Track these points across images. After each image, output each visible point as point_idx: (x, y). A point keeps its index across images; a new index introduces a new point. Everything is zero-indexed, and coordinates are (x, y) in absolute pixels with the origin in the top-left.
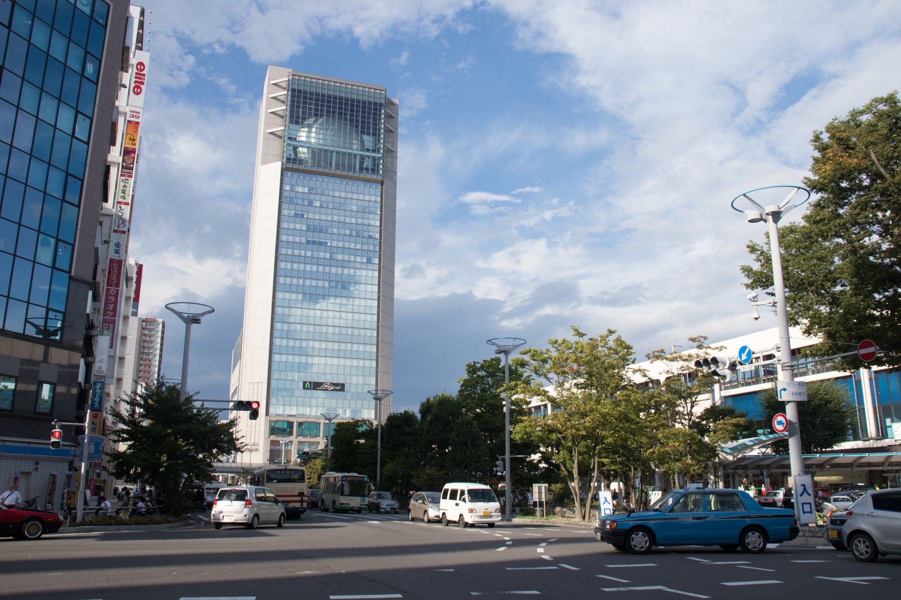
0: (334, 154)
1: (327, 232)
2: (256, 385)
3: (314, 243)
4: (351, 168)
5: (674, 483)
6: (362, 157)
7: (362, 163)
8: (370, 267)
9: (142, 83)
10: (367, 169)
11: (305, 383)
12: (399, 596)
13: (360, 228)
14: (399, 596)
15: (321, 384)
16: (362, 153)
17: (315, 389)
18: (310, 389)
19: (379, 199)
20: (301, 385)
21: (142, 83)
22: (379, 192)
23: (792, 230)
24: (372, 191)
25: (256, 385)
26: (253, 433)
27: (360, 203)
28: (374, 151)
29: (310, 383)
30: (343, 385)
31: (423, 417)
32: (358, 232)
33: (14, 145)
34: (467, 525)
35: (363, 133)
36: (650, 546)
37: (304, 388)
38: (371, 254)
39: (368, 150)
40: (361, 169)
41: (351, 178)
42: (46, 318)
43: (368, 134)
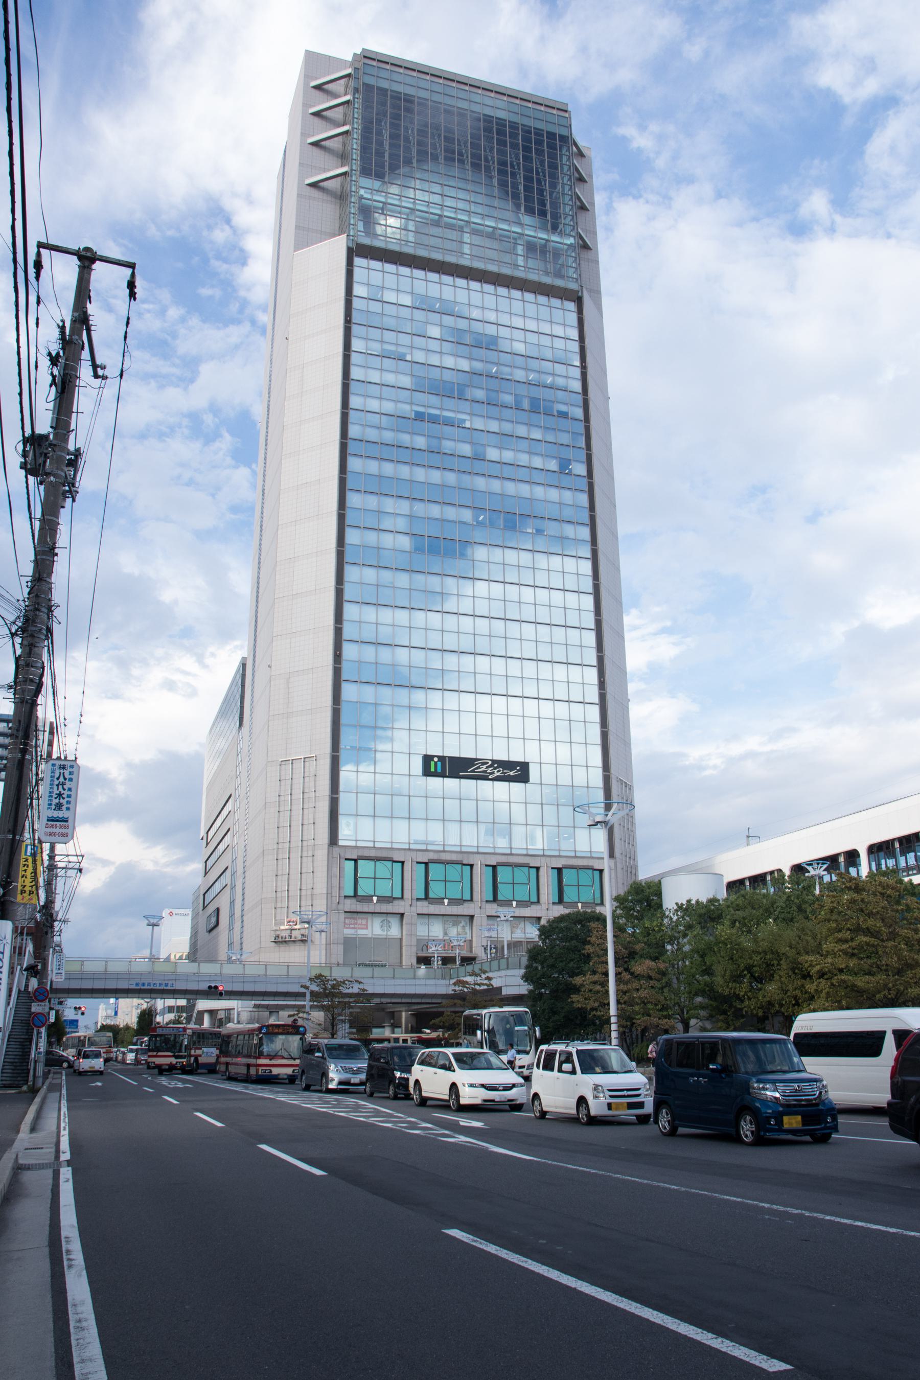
1: (461, 398)
2: (299, 766)
3: (434, 420)
8: (566, 481)
11: (427, 759)
13: (540, 393)
15: (469, 762)
17: (454, 775)
18: (442, 775)
19: (574, 334)
20: (417, 765)
22: (573, 318)
23: (544, 926)
24: (558, 315)
25: (299, 766)
26: (298, 795)
27: (532, 338)
29: (442, 759)
31: (544, 941)
32: (535, 402)
34: (594, 1121)
37: (427, 772)
38: (569, 454)
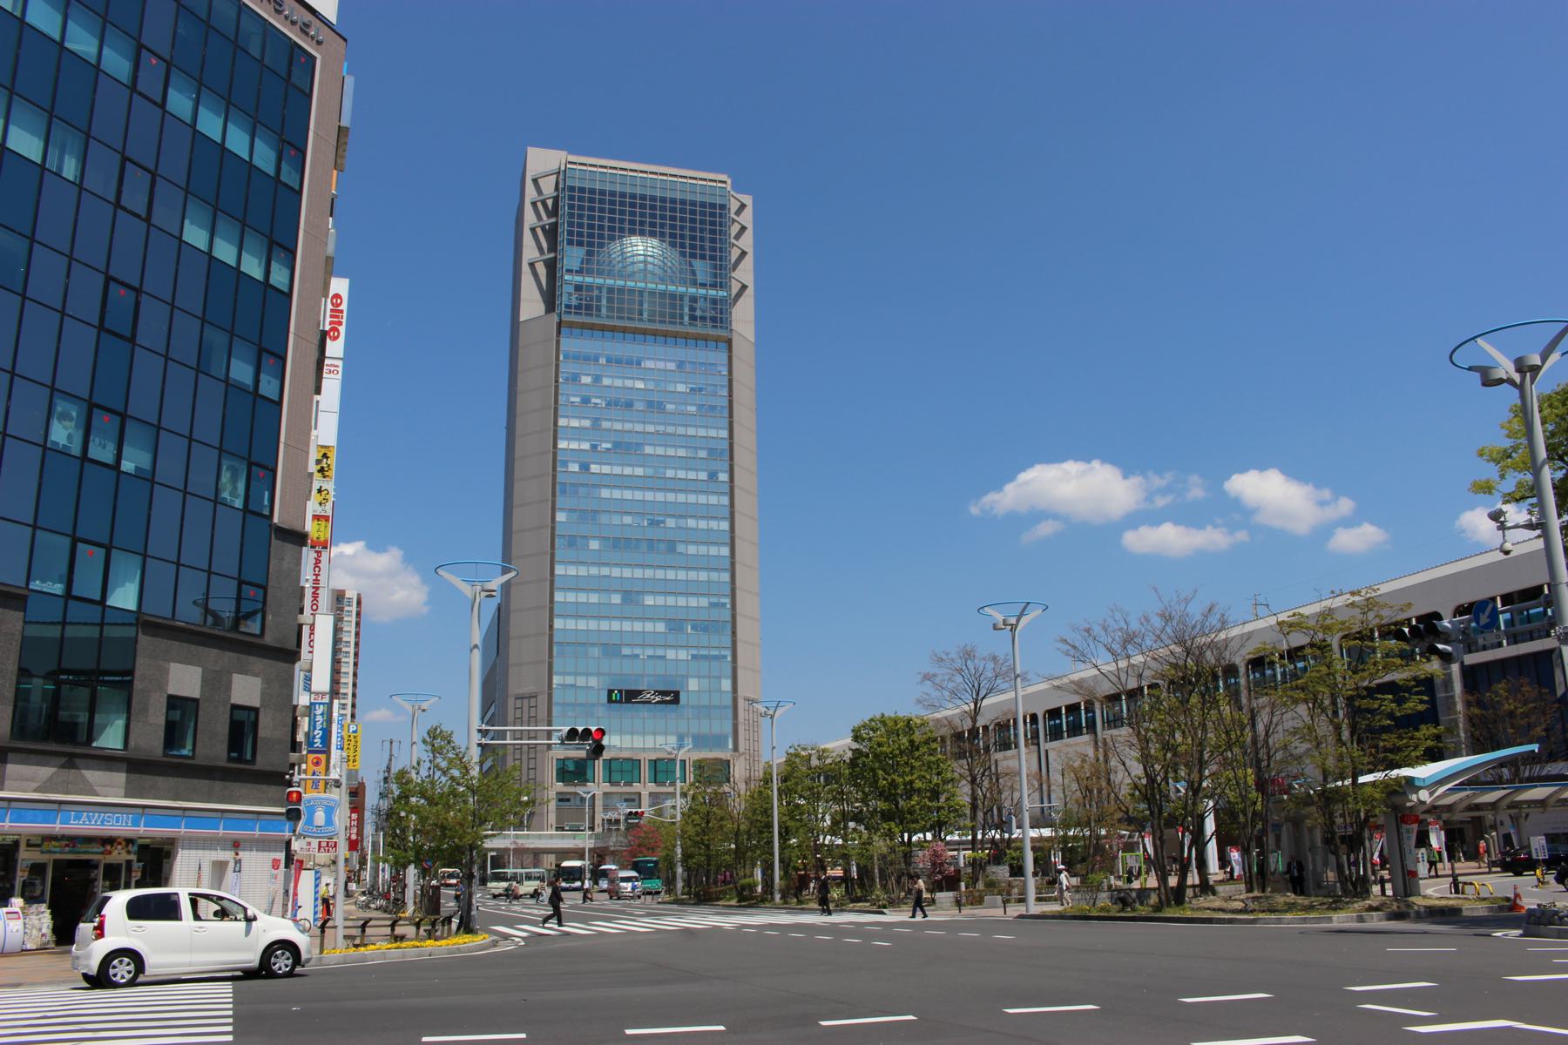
0: (646, 295)
4: (675, 317)
5: (1305, 920)
6: (694, 299)
7: (692, 309)
9: (340, 323)
10: (703, 318)
11: (610, 692)
12: (628, 1032)
14: (628, 1032)
15: (639, 692)
16: (692, 290)
17: (628, 701)
20: (604, 698)
21: (340, 323)
28: (713, 286)
30: (677, 694)
33: (168, 308)
35: (693, 256)
36: (136, 976)
37: (610, 700)
39: (703, 285)
40: (693, 318)
41: (676, 335)
42: (239, 599)
43: (703, 257)
